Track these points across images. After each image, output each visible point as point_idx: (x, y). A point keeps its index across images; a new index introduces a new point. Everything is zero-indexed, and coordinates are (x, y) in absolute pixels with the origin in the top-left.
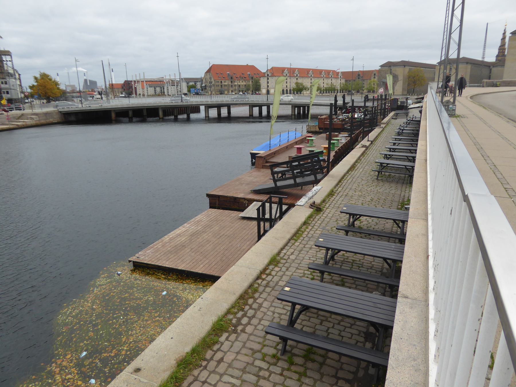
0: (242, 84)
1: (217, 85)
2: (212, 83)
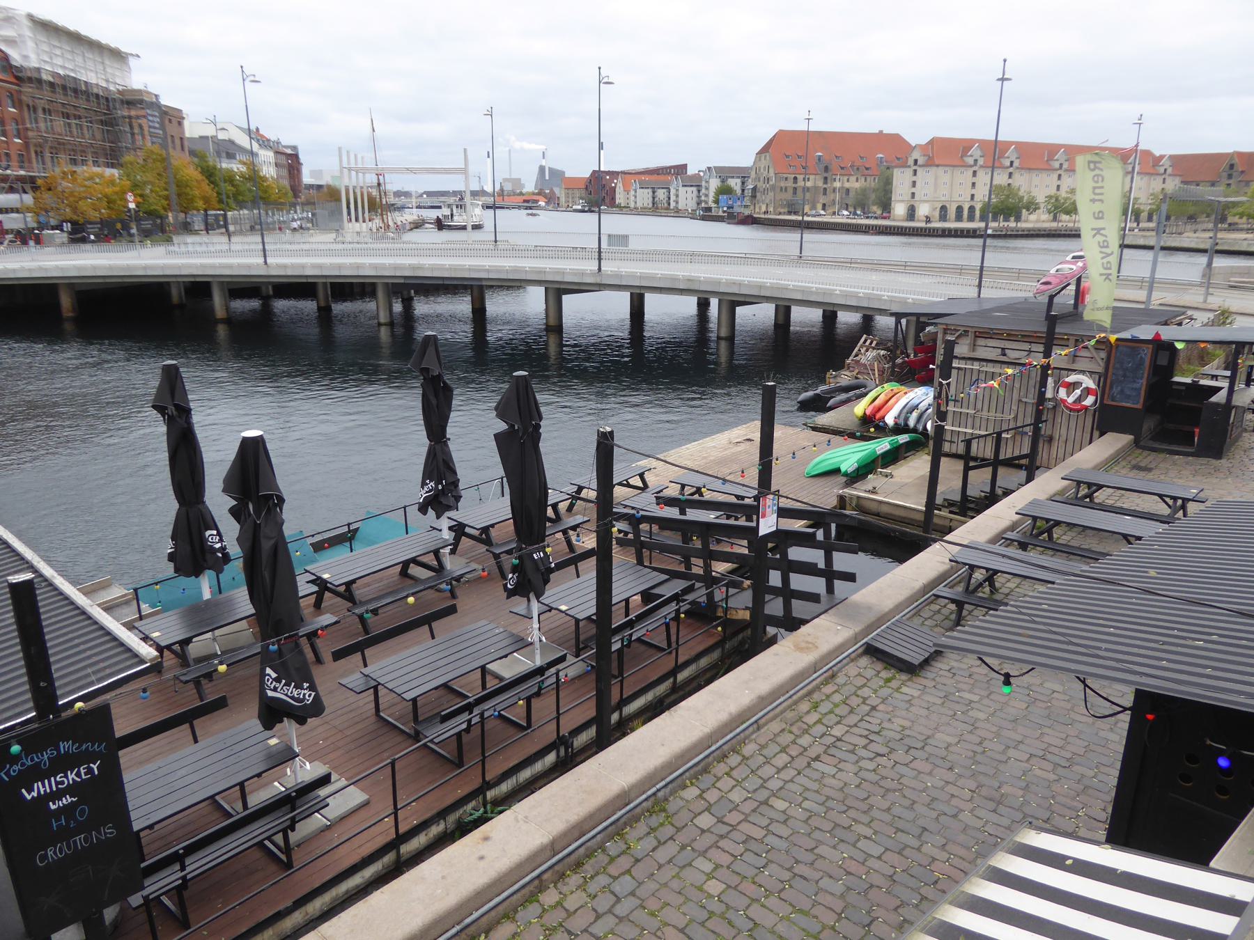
1: (781, 188)
2: (771, 183)
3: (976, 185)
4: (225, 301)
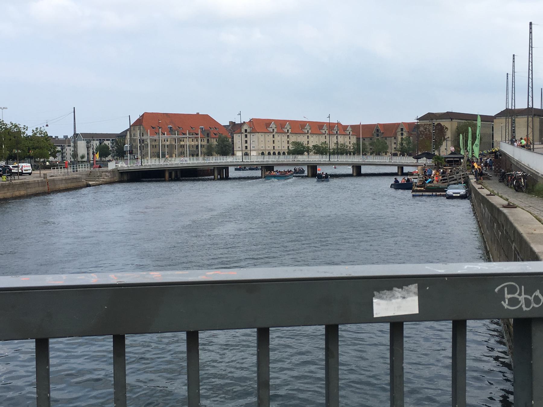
3: (275, 142)
4: (443, 196)
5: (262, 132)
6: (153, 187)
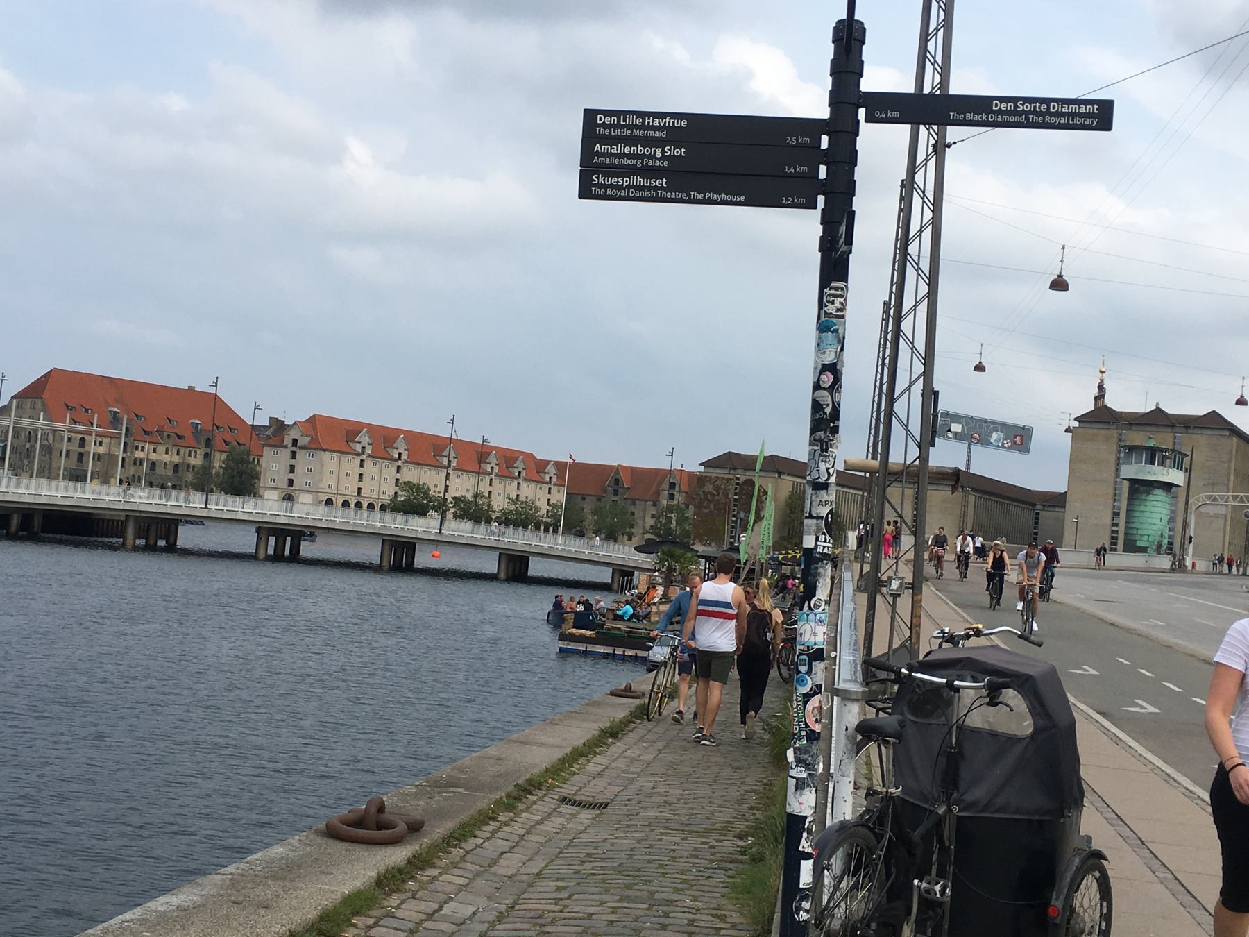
0: (167, 458)
3: (364, 477)
5: (334, 451)
6: (494, 596)
